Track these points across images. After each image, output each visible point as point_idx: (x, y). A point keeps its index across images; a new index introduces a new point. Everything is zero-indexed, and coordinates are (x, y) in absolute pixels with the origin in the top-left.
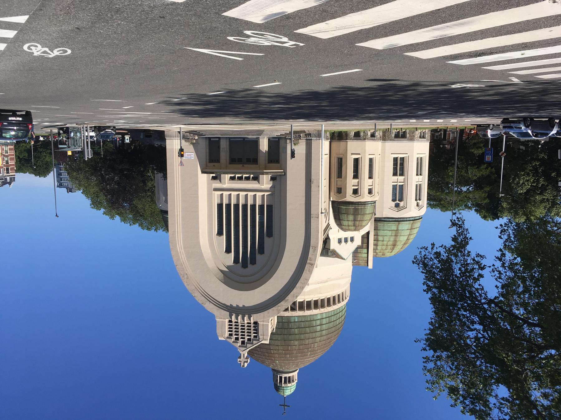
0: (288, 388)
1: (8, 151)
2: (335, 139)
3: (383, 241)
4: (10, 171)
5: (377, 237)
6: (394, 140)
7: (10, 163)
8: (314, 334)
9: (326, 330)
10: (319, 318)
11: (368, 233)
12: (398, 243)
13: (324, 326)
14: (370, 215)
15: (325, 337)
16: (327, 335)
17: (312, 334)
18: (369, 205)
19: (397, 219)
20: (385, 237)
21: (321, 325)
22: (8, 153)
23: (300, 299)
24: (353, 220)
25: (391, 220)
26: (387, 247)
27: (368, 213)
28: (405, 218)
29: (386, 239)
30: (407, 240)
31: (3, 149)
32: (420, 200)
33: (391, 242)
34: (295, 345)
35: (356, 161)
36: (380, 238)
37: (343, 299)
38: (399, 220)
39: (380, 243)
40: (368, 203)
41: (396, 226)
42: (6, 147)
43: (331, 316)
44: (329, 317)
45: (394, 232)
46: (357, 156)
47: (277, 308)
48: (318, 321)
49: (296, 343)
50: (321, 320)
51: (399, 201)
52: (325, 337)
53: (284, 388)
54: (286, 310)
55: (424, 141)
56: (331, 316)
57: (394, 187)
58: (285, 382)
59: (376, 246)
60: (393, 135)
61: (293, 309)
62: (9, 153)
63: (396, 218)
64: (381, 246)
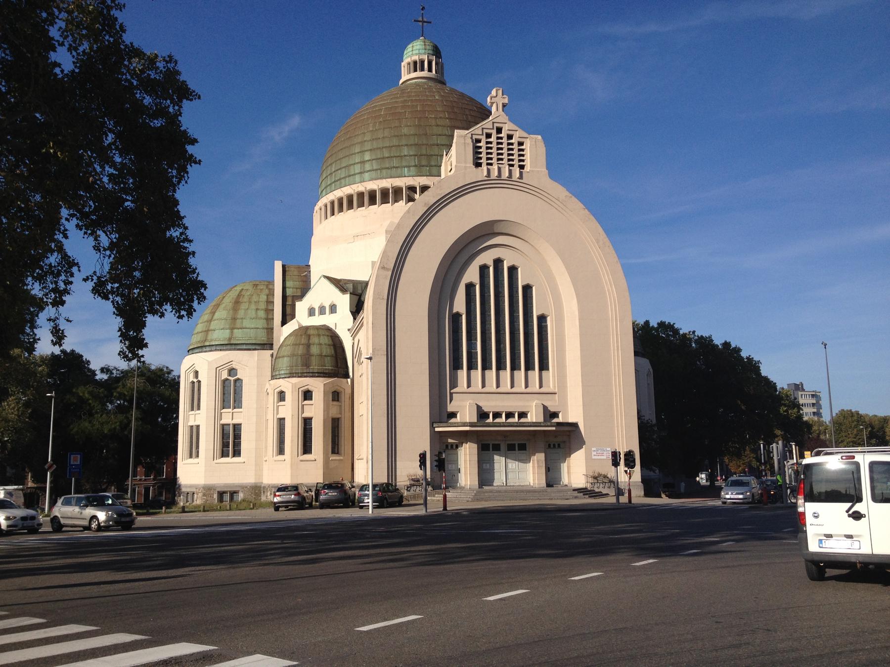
0: (417, 52)
3: (257, 309)
5: (267, 316)
8: (375, 146)
9: (354, 152)
11: (284, 322)
17: (379, 146)
21: (363, 162)
23: (402, 206)
24: (312, 346)
25: (244, 347)
26: (250, 299)
27: (285, 358)
29: (252, 313)
32: (193, 383)
33: (243, 308)
35: (307, 448)
36: (262, 314)
38: (229, 347)
39: (263, 306)
41: (234, 336)
43: (345, 178)
44: (350, 176)
53: (424, 51)
54: (424, 189)
56: (345, 178)
58: (422, 62)
61: (412, 189)
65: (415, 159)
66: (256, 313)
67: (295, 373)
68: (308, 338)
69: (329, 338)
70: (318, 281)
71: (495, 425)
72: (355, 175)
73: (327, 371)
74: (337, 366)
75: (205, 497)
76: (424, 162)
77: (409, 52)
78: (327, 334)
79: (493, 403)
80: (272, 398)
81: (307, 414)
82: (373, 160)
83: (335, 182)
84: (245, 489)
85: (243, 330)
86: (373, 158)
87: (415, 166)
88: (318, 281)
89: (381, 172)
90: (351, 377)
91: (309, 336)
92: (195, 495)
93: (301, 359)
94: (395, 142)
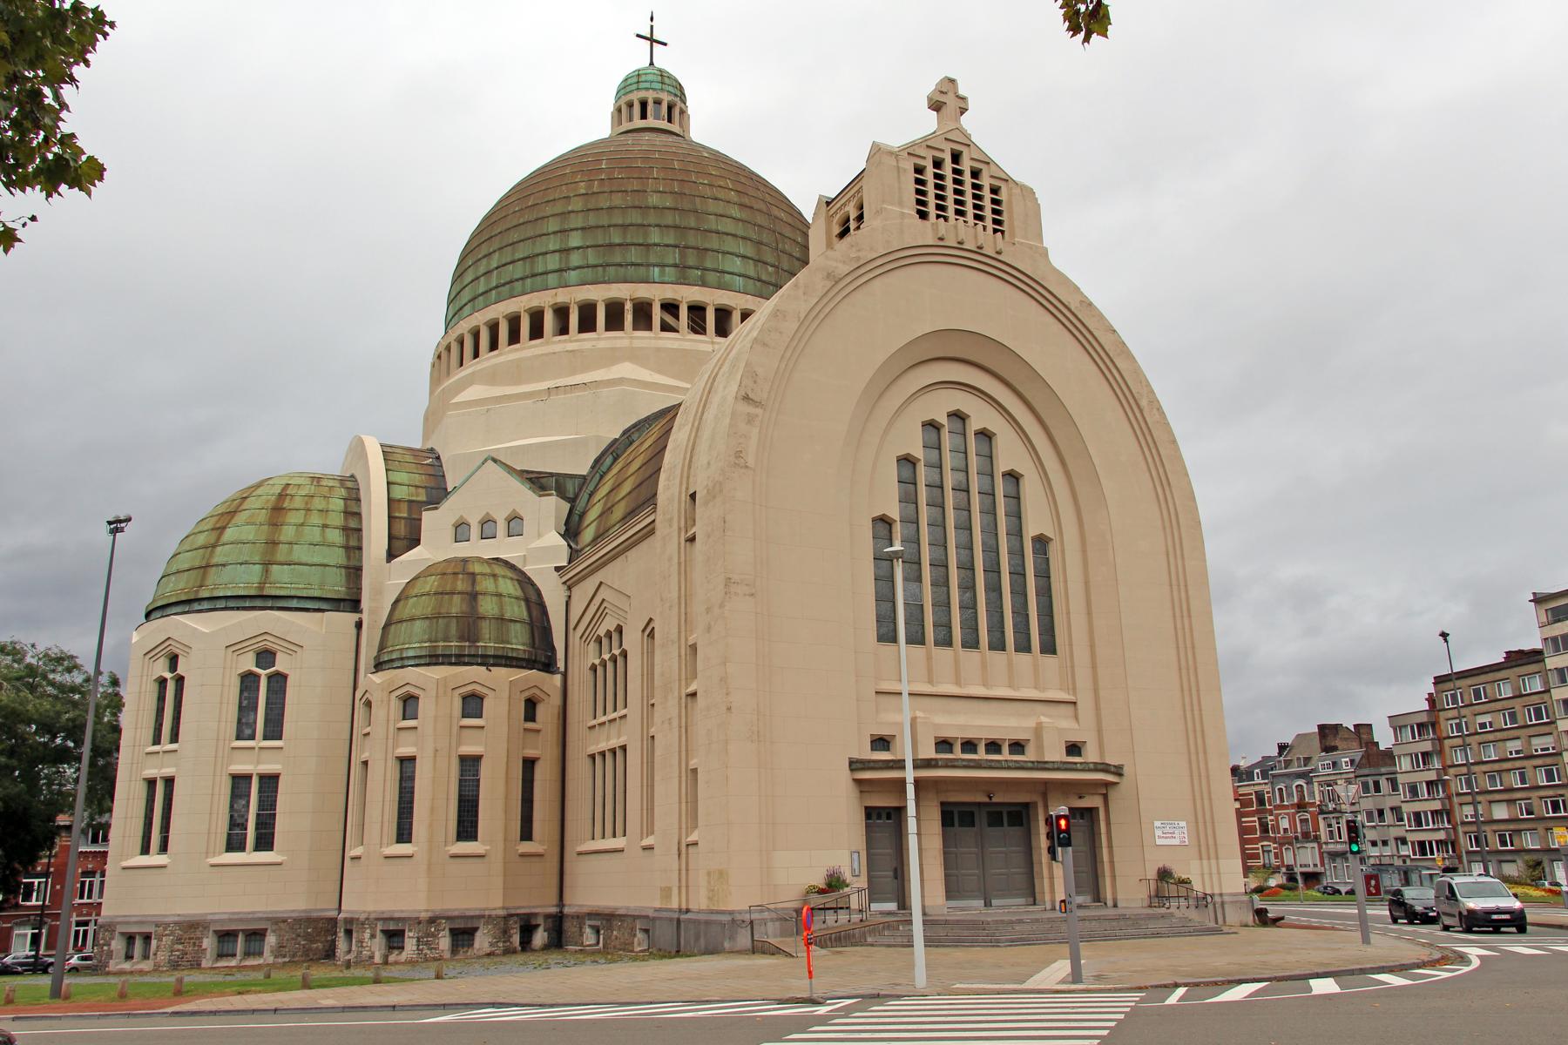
1: (1260, 851)
2: (547, 916)
3: (325, 526)
4: (1253, 797)
5: (348, 540)
6: (268, 919)
7: (1256, 819)
9: (545, 232)
10: (573, 273)
12: (263, 516)
13: (551, 247)
14: (405, 616)
15: (549, 210)
16: (543, 218)
17: (601, 224)
18: (411, 653)
19: (269, 604)
20: (317, 539)
21: (566, 251)
22: (1262, 846)
24: (480, 597)
25: (294, 603)
27: (418, 623)
28: (232, 609)
29: (314, 534)
30: (223, 528)
31: (1276, 857)
33: (292, 521)
34: (660, 192)
35: (467, 828)
36: (336, 536)
37: (461, 343)
38: (258, 603)
39: (337, 519)
40: (417, 662)
41: (272, 579)
42: (1267, 861)
44: (534, 275)
45: (280, 557)
46: (526, 847)
47: (860, 254)
48: (576, 264)
49: (654, 200)
50: (563, 266)
51: (258, 676)
52: (549, 210)
55: (128, 923)
57: (274, 729)
59: (349, 510)
60: (271, 940)
62: (1259, 846)
63: (271, 608)
64: (331, 507)
65: (675, 253)
66: (323, 534)
67: (443, 656)
68: (470, 582)
69: (516, 583)
70: (479, 467)
71: (991, 766)
72: (546, 273)
73: (514, 655)
74: (533, 645)
75: (180, 947)
76: (691, 261)
77: (630, 85)
78: (515, 577)
79: (961, 720)
80: (387, 711)
81: (469, 749)
82: (588, 247)
83: (497, 287)
84: (282, 925)
85: (293, 567)
86: (588, 244)
87: (675, 266)
88: (479, 467)
89: (604, 271)
90: (562, 669)
91: (473, 574)
92: (154, 943)
93: (457, 626)
94: (634, 217)
